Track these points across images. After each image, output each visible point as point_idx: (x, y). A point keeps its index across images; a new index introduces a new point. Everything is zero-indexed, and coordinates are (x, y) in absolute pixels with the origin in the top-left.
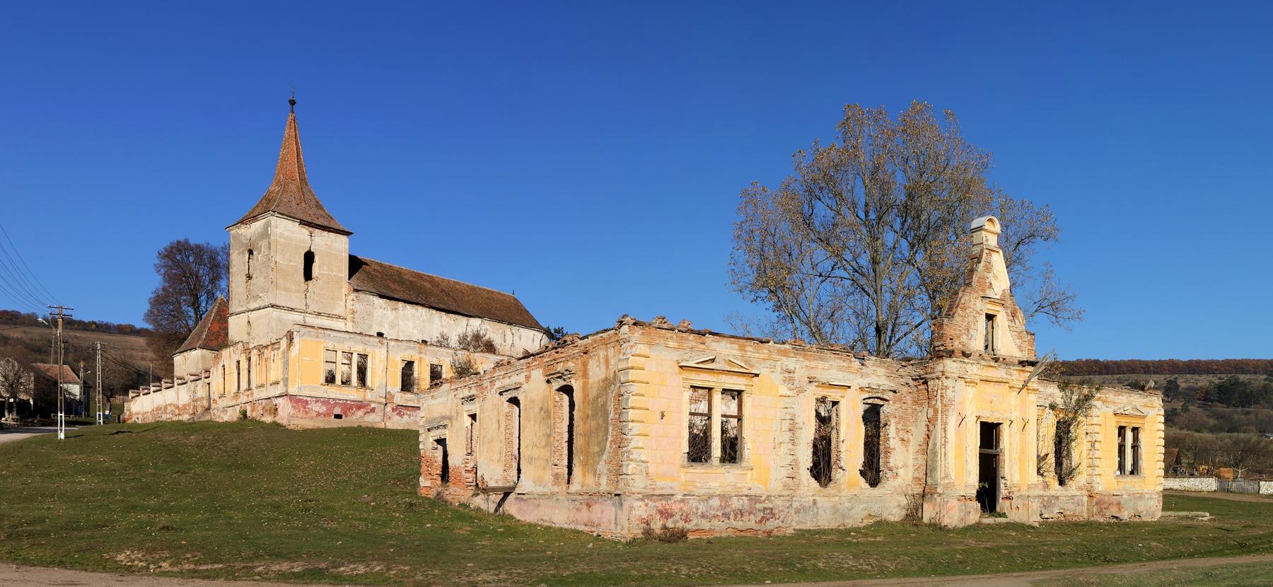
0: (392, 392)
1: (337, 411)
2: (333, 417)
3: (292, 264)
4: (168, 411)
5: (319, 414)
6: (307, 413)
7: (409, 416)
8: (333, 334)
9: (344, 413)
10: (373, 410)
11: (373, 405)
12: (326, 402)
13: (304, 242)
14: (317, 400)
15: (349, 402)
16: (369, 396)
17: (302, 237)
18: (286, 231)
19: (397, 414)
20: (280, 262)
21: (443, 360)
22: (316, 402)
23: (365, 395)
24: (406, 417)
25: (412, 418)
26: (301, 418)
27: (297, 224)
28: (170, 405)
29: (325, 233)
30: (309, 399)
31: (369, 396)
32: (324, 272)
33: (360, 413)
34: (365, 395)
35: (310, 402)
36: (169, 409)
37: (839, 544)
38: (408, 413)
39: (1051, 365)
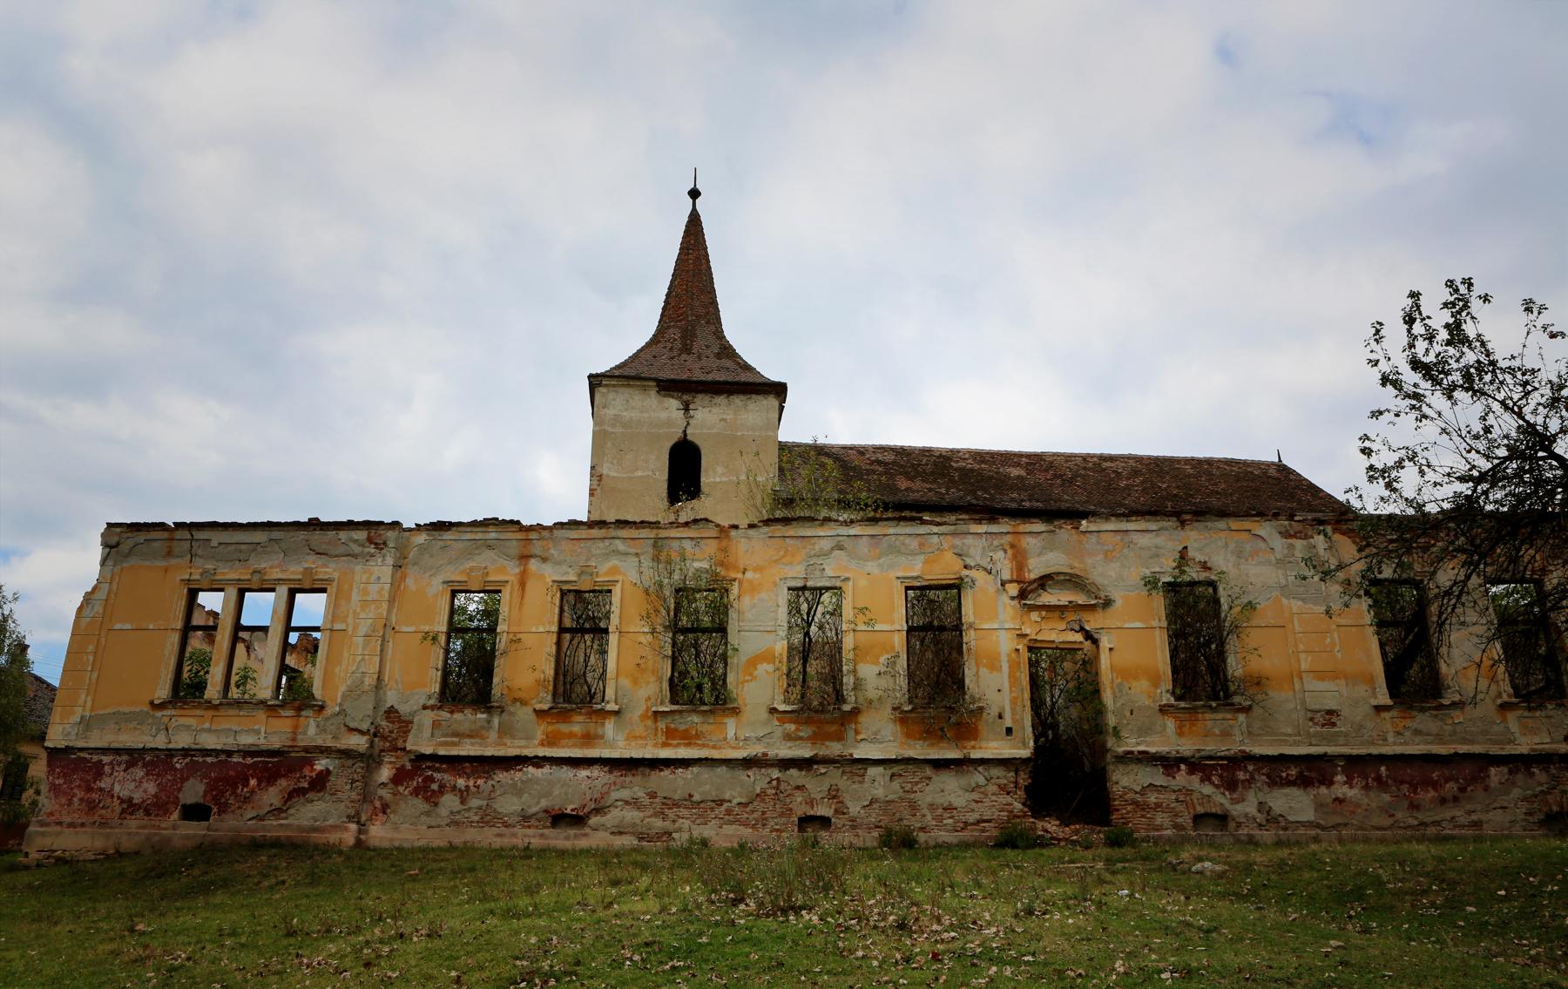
0: (404, 709)
1: (194, 791)
2: (175, 815)
3: (639, 473)
5: (129, 807)
6: (92, 807)
7: (464, 795)
8: (216, 537)
9: (216, 800)
10: (320, 782)
11: (321, 764)
12: (157, 761)
13: (669, 423)
14: (134, 756)
15: (236, 759)
16: (312, 730)
17: (663, 415)
18: (626, 410)
19: (416, 792)
20: (612, 474)
21: (614, 570)
22: (130, 765)
23: (296, 727)
24: (449, 802)
25: (475, 803)
26: (72, 825)
27: (653, 393)
29: (721, 399)
30: (106, 759)
31: (312, 730)
32: (718, 480)
33: (272, 796)
34: (296, 727)
35: (107, 769)
37: (828, 455)
38: (461, 782)
39: (1536, 734)
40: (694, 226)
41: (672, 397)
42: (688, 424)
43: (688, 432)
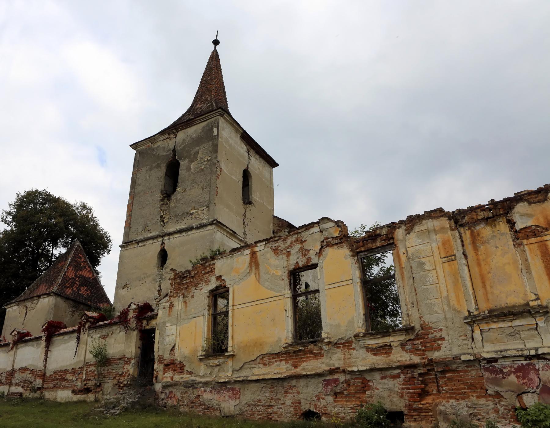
4: (14, 381)
28: (23, 370)
36: (18, 377)
40: (215, 58)
41: (244, 143)
42: (249, 162)
43: (249, 166)
